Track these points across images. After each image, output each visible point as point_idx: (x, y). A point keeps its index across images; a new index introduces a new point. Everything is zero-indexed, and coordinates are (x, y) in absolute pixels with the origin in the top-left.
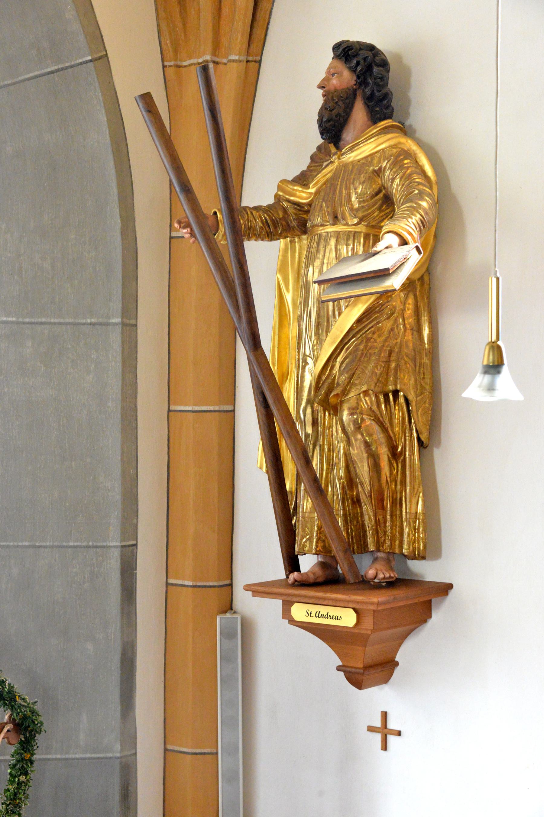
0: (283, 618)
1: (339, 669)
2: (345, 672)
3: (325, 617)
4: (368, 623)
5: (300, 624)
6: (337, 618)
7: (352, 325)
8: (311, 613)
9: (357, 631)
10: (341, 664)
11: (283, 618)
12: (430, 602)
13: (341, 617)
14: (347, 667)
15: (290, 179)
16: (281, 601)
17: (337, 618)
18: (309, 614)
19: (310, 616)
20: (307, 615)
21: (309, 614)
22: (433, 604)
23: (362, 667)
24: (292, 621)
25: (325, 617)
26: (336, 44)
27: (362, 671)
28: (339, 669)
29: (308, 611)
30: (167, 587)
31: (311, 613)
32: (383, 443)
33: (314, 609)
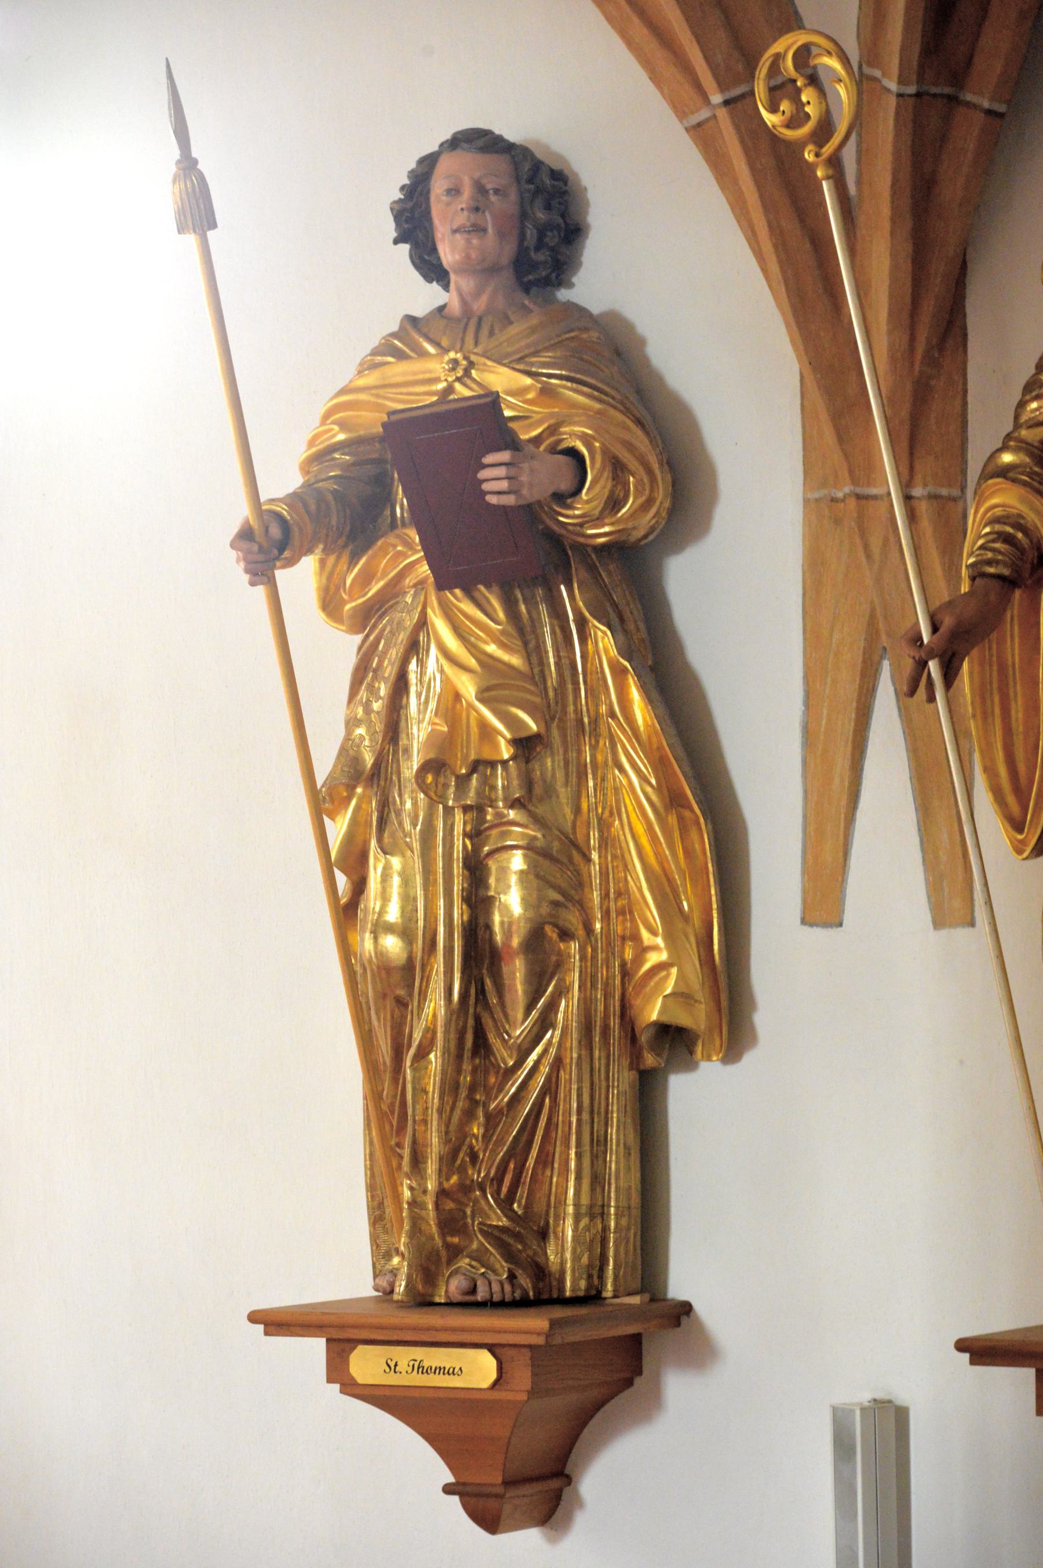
0: (330, 1380)
1: (448, 1490)
2: (462, 1495)
3: (427, 1371)
4: (522, 1378)
5: (366, 1392)
6: (452, 1372)
7: (899, 1542)
8: (396, 1365)
9: (496, 1395)
10: (451, 1479)
11: (330, 1380)
12: (635, 1341)
13: (460, 1369)
14: (464, 1484)
15: (318, 425)
16: (323, 1341)
17: (452, 1372)
18: (392, 1367)
19: (395, 1372)
20: (388, 1370)
21: (393, 1368)
22: (644, 1340)
23: (500, 1480)
24: (351, 1388)
25: (440, 1368)
26: (421, 158)
27: (500, 1490)
28: (448, 1490)
29: (389, 1361)
30: (485, 1277)
31: (396, 1365)
32: (518, 953)
33: (404, 1356)
